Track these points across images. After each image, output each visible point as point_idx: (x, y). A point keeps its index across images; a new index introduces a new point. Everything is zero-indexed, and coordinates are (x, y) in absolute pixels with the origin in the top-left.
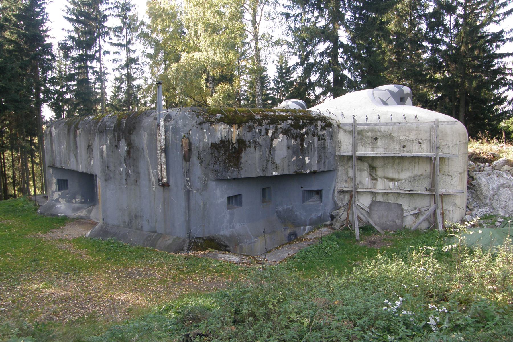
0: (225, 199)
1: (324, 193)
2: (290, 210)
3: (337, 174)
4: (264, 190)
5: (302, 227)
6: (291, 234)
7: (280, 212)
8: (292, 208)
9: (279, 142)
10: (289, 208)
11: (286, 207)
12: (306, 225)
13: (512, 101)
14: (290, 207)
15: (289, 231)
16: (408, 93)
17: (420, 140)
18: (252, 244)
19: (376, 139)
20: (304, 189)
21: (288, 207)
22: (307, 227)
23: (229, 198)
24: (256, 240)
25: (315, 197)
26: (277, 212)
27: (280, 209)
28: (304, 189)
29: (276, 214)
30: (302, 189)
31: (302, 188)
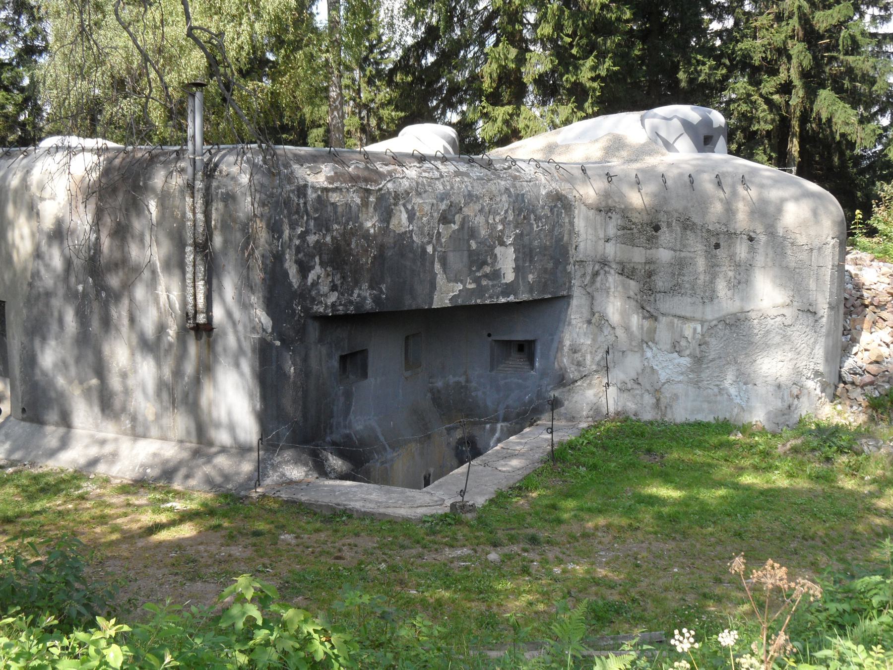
0: (335, 363)
1: (539, 349)
2: (462, 387)
3: (569, 304)
4: (407, 338)
5: (488, 426)
6: (461, 442)
7: (439, 391)
8: (467, 381)
9: (454, 232)
10: (458, 383)
11: (452, 379)
12: (496, 420)
13: (333, 5)
14: (462, 379)
15: (458, 434)
16: (720, 127)
17: (751, 234)
18: (387, 465)
19: (657, 228)
20: (494, 338)
21: (457, 379)
22: (499, 426)
23: (343, 359)
24: (395, 454)
25: (516, 361)
26: (431, 390)
27: (439, 384)
28: (494, 338)
29: (429, 395)
30: (490, 339)
31: (489, 335)
